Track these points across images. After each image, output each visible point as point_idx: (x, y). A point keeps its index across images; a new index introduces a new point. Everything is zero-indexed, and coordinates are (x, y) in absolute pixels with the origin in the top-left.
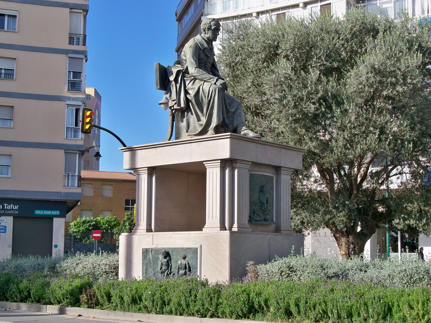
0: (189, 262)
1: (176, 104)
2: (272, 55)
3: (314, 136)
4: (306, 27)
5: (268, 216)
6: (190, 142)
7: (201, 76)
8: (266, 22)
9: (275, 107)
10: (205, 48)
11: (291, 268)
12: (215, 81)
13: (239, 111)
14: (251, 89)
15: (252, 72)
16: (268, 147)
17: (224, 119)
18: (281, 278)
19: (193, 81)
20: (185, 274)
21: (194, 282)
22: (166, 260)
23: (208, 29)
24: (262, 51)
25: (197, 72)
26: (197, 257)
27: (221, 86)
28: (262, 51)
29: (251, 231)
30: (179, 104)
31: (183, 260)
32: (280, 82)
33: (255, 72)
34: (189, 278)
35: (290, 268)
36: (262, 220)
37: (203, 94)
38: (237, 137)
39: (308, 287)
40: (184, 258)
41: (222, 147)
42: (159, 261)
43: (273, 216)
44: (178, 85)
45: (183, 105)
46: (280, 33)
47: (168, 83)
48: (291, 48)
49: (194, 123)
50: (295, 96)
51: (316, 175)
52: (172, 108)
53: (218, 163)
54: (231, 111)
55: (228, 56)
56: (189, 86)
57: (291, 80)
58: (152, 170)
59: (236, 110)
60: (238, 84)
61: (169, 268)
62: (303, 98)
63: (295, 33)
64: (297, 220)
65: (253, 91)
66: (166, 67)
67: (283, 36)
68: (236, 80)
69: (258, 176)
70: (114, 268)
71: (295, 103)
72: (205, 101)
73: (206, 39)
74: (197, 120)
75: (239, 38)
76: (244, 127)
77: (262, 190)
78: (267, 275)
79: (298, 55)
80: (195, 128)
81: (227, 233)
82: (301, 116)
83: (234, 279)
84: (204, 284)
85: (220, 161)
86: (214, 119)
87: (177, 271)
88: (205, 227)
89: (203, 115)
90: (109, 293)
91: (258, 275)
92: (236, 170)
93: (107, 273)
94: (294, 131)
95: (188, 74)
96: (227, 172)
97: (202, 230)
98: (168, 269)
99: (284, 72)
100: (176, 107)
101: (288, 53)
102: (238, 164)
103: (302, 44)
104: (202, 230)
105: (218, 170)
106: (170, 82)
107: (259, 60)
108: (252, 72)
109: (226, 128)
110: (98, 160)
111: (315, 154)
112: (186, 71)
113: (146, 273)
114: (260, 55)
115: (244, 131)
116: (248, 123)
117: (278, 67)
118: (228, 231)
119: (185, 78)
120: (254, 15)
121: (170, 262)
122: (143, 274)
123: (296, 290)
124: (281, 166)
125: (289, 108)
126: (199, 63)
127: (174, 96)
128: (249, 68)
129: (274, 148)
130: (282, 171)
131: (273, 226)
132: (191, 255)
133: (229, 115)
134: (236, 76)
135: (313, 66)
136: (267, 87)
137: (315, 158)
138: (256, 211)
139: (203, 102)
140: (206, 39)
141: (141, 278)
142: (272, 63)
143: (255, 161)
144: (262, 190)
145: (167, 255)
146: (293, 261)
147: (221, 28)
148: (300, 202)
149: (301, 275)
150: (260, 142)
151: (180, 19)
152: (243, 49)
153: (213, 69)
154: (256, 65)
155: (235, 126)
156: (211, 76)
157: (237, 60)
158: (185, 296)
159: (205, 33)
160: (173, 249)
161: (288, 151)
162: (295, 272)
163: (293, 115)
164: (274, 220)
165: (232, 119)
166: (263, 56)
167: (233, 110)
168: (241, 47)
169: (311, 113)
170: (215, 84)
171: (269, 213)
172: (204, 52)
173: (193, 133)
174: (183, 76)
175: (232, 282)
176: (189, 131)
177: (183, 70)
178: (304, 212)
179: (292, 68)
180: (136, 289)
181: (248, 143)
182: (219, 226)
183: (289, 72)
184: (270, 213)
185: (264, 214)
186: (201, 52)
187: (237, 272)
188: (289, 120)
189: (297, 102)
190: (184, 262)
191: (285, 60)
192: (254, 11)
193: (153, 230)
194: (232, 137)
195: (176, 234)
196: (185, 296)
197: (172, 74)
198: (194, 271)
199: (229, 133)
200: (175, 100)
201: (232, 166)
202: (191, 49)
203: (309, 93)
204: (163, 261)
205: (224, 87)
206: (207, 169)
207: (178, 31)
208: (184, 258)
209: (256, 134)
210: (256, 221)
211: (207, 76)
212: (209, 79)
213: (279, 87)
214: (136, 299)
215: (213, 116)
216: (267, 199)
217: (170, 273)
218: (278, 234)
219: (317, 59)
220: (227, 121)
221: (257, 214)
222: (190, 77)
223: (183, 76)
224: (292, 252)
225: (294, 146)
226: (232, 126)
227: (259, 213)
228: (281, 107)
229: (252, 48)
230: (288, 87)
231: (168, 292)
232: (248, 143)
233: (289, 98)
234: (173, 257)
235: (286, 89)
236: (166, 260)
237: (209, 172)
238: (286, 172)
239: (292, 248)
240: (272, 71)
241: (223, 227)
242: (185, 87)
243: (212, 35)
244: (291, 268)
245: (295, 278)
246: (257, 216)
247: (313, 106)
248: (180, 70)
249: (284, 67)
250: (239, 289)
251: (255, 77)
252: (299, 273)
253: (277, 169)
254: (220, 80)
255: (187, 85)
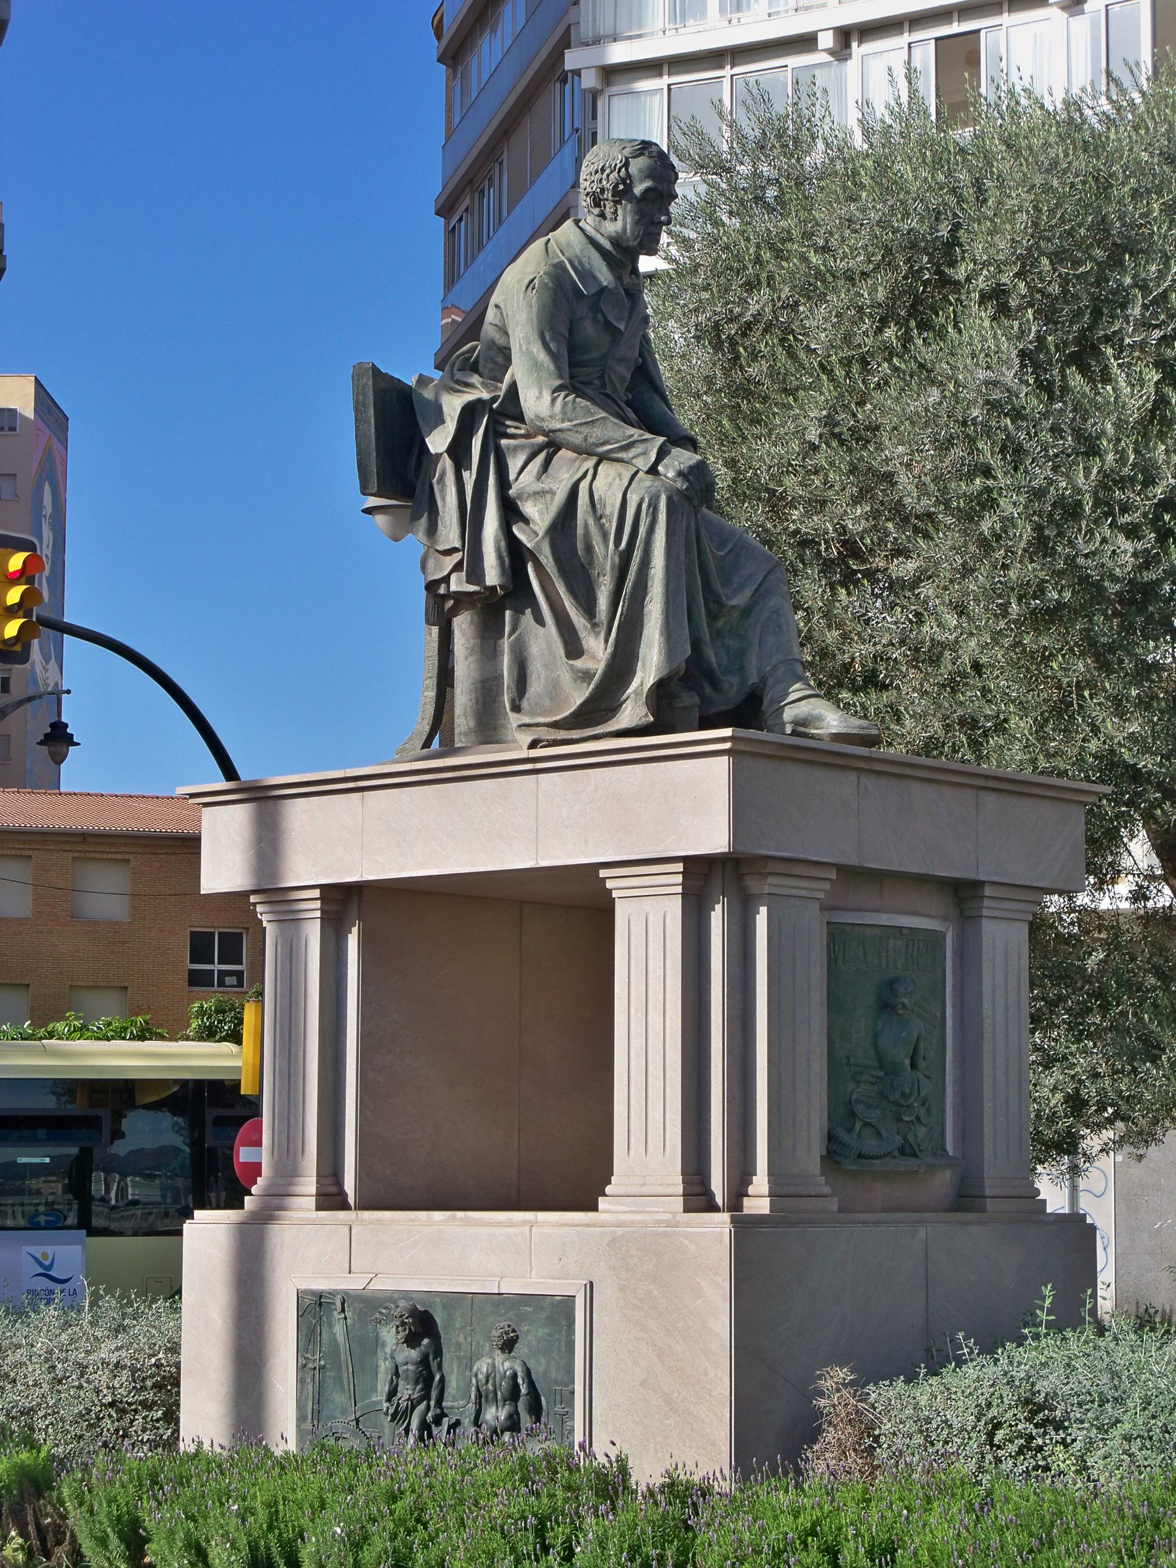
0: (531, 1364)
1: (458, 567)
2: (923, 293)
3: (1134, 693)
4: (1094, 146)
5: (922, 1131)
6: (532, 768)
7: (585, 430)
8: (889, 121)
10: (603, 289)
11: (1041, 1408)
12: (653, 456)
13: (773, 602)
14: (820, 459)
16: (916, 788)
17: (696, 644)
18: (989, 1457)
19: (541, 457)
20: (513, 1425)
21: (563, 1474)
22: (414, 1354)
24: (877, 268)
25: (563, 411)
26: (571, 1344)
27: (681, 485)
28: (877, 268)
29: (835, 1208)
30: (475, 572)
31: (499, 1357)
33: (839, 372)
34: (535, 1449)
35: (1036, 1408)
36: (889, 1154)
37: (591, 521)
38: (767, 750)
39: (1130, 1523)
40: (508, 1345)
41: (690, 799)
42: (380, 1355)
43: (943, 1124)
44: (470, 478)
45: (492, 577)
46: (963, 176)
47: (419, 463)
50: (1039, 494)
51: (1143, 865)
52: (442, 590)
53: (674, 878)
54: (734, 602)
55: (706, 288)
56: (524, 480)
57: (1017, 415)
58: (342, 901)
59: (759, 596)
60: (756, 430)
61: (434, 1394)
62: (1079, 504)
63: (1038, 180)
64: (1050, 1091)
65: (832, 464)
66: (411, 381)
67: (980, 189)
68: (744, 406)
69: (868, 931)
70: (158, 1386)
71: (1038, 528)
72: (605, 557)
73: (607, 245)
74: (562, 652)
75: (757, 199)
76: (797, 686)
77: (886, 1003)
78: (919, 1440)
79: (1055, 289)
80: (555, 692)
81: (721, 1222)
82: (1067, 595)
83: (760, 1464)
84: (612, 1485)
85: (680, 867)
86: (650, 646)
87: (471, 1407)
88: (608, 1190)
90: (136, 1523)
91: (876, 1439)
92: (763, 910)
93: (123, 1411)
95: (520, 418)
96: (717, 918)
97: (595, 1208)
98: (427, 1397)
100: (458, 584)
102: (770, 880)
103: (1070, 233)
104: (595, 1208)
105: (674, 908)
107: (860, 309)
109: (708, 690)
110: (59, 759)
111: (1135, 775)
112: (511, 406)
113: (317, 1414)
118: (725, 1217)
119: (504, 442)
120: (826, 40)
121: (434, 1365)
122: (301, 1418)
123: (1067, 1532)
124: (983, 877)
126: (572, 365)
127: (450, 533)
128: (808, 349)
129: (946, 790)
130: (986, 903)
131: (943, 1182)
132: (542, 1332)
133: (720, 623)
134: (745, 390)
135: (1127, 341)
137: (1139, 795)
138: (859, 1108)
139: (591, 562)
141: (292, 1446)
143: (854, 861)
144: (886, 1003)
145: (421, 1325)
146: (1047, 1362)
147: (674, 160)
148: (1061, 999)
149: (1090, 1444)
151: (455, 55)
152: (779, 255)
153: (639, 399)
154: (847, 339)
155: (753, 678)
156: (631, 431)
157: (753, 308)
158: (513, 1550)
159: (602, 216)
160: (453, 1300)
161: (1015, 800)
162: (1059, 1426)
164: (949, 1148)
166: (881, 295)
167: (739, 600)
168: (772, 247)
169: (1115, 579)
170: (653, 471)
171: (922, 1113)
173: (545, 713)
174: (495, 433)
175: (745, 1478)
176: (525, 704)
177: (494, 399)
178: (1085, 1051)
179: (1022, 354)
180: (271, 1505)
181: (819, 774)
182: (680, 1189)
183: (1009, 376)
184: (928, 1112)
185: (900, 1120)
186: (582, 310)
187: (773, 1428)
190: (505, 1365)
191: (986, 314)
192: (823, 21)
193: (351, 1200)
194: (741, 747)
195: (466, 1223)
196: (513, 1550)
197: (440, 420)
198: (558, 1409)
199: (728, 732)
200: (454, 550)
201: (744, 889)
202: (533, 295)
203: (1109, 481)
204: (400, 1359)
205: (697, 488)
206: (618, 904)
208: (508, 1345)
210: (860, 1156)
211: (613, 431)
213: (958, 452)
214: (269, 1558)
215: (646, 632)
216: (916, 1048)
217: (438, 1421)
218: (972, 1216)
219: (1145, 307)
220: (711, 655)
221: (866, 1124)
222: (527, 436)
223: (495, 433)
224: (1043, 1316)
226: (735, 680)
227: (874, 1115)
228: (973, 548)
231: (431, 1528)
234: (453, 1338)
235: (996, 462)
236: (414, 1354)
237: (628, 918)
238: (1007, 905)
239: (1043, 1299)
241: (698, 1197)
242: (504, 484)
243: (637, 223)
244: (1041, 1408)
245: (1061, 1459)
246: (867, 1132)
247: (1126, 545)
248: (480, 400)
249: (982, 351)
250: (786, 1521)
252: (1081, 1435)
253: (963, 894)
254: (676, 451)
255: (512, 477)
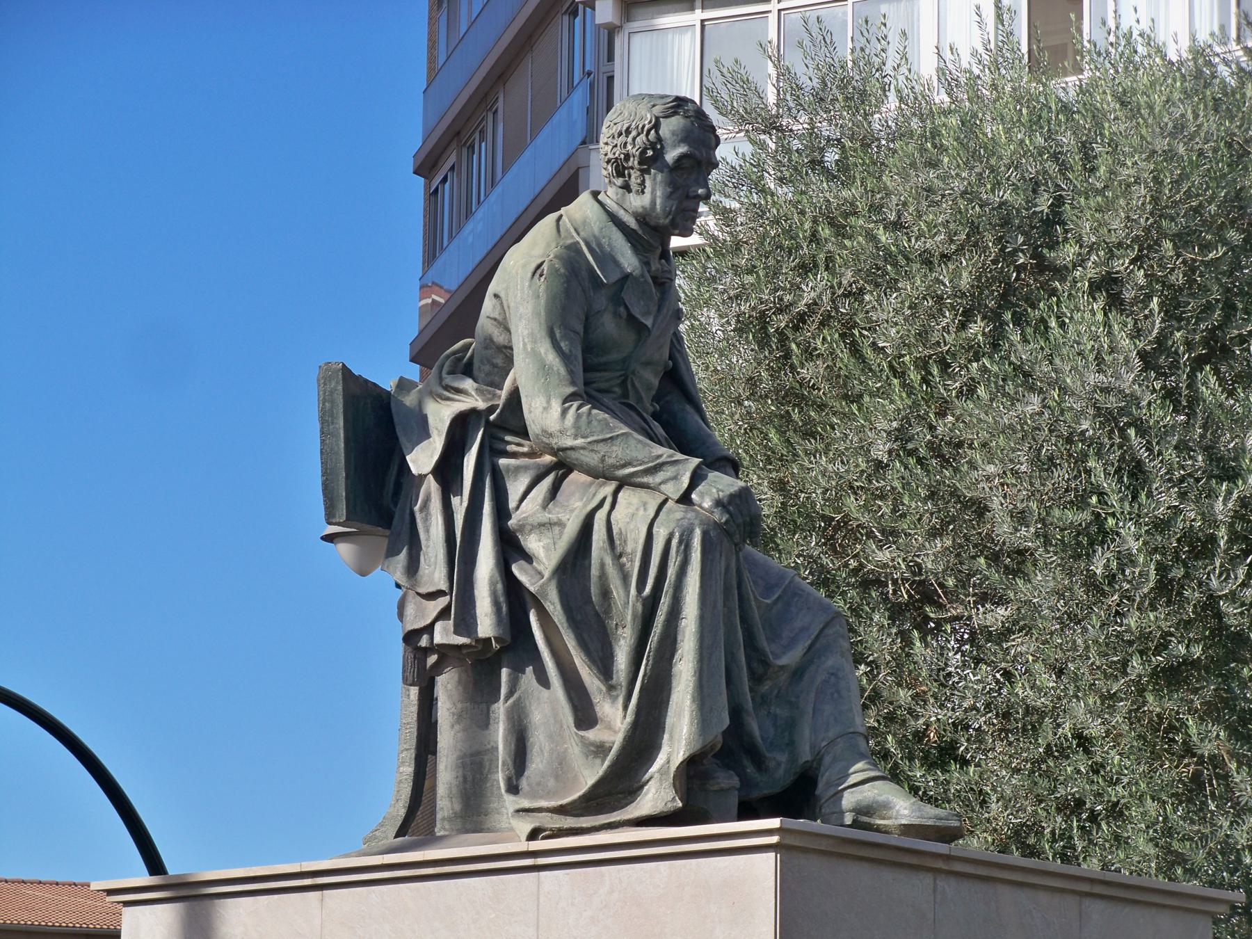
1: (444, 614)
6: (529, 863)
7: (602, 448)
9: (1042, 584)
10: (626, 277)
12: (685, 481)
14: (893, 479)
15: (901, 374)
16: (1005, 893)
17: (736, 713)
23: (643, 160)
24: (960, 249)
25: (576, 425)
27: (719, 516)
30: (466, 622)
32: (1069, 440)
37: (608, 560)
38: (823, 845)
44: (460, 505)
45: (486, 626)
46: (1067, 139)
48: (1136, 239)
49: (556, 737)
50: (1161, 526)
52: (424, 642)
54: (783, 661)
55: (751, 270)
56: (527, 507)
59: (813, 654)
60: (810, 445)
62: (1213, 539)
63: (1161, 144)
68: (795, 416)
71: (1162, 569)
73: (632, 223)
76: (860, 765)
80: (561, 767)
86: (679, 715)
89: (611, 688)
94: (1161, 738)
95: (523, 432)
99: (1093, 378)
100: (444, 634)
101: (1121, 265)
103: (1197, 210)
106: (406, 482)
107: (939, 299)
108: (901, 374)
109: (750, 770)
112: (511, 418)
114: (944, 274)
115: (863, 790)
116: (871, 676)
117: (1057, 347)
119: (503, 462)
125: (1127, 596)
126: (586, 369)
127: (434, 572)
129: (1043, 897)
133: (765, 687)
134: (796, 396)
136: (991, 469)
139: (608, 610)
140: (632, 223)
142: (1018, 320)
150: (958, 867)
152: (840, 231)
153: (669, 410)
154: (923, 335)
155: (806, 755)
156: (659, 450)
157: (808, 297)
159: (626, 187)
161: (1128, 909)
163: (1147, 644)
165: (781, 712)
166: (965, 281)
167: (790, 659)
168: (832, 223)
170: (685, 499)
172: (617, 299)
173: (549, 795)
174: (492, 450)
176: (524, 783)
177: (491, 410)
179: (1142, 355)
183: (1127, 380)
186: (601, 301)
188: (1125, 673)
189: (1177, 558)
194: (791, 841)
197: (423, 432)
199: (775, 823)
200: (440, 593)
202: (541, 283)
205: (739, 522)
207: (432, 45)
209: (931, 810)
211: (639, 450)
212: (648, 472)
213: (1062, 474)
220: (753, 726)
223: (492, 450)
225: (1162, 882)
226: (783, 758)
229: (897, 226)
230: (1118, 471)
232: (888, 875)
233: (1131, 538)
240: (1024, 374)
242: (502, 513)
243: (669, 197)
248: (473, 411)
251: (916, 404)
254: (713, 475)
255: (512, 504)
